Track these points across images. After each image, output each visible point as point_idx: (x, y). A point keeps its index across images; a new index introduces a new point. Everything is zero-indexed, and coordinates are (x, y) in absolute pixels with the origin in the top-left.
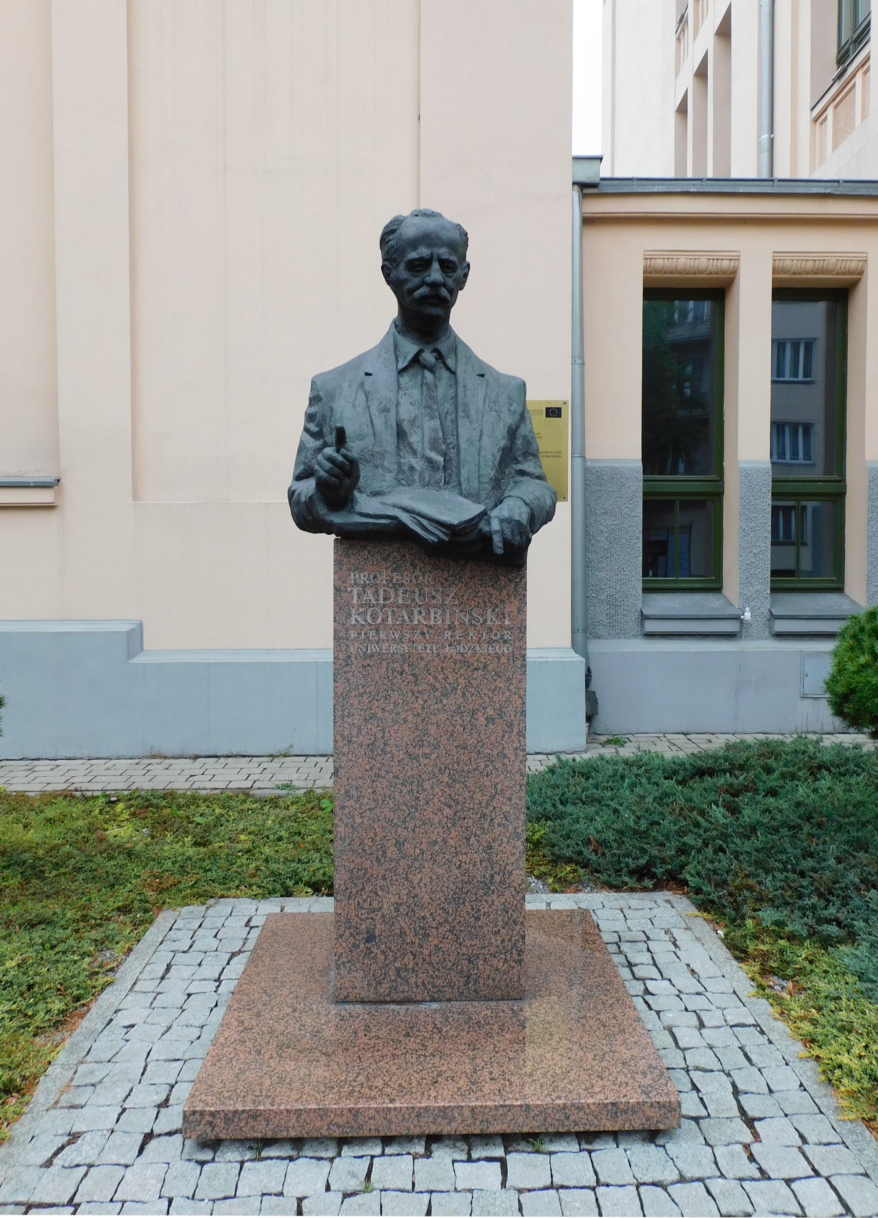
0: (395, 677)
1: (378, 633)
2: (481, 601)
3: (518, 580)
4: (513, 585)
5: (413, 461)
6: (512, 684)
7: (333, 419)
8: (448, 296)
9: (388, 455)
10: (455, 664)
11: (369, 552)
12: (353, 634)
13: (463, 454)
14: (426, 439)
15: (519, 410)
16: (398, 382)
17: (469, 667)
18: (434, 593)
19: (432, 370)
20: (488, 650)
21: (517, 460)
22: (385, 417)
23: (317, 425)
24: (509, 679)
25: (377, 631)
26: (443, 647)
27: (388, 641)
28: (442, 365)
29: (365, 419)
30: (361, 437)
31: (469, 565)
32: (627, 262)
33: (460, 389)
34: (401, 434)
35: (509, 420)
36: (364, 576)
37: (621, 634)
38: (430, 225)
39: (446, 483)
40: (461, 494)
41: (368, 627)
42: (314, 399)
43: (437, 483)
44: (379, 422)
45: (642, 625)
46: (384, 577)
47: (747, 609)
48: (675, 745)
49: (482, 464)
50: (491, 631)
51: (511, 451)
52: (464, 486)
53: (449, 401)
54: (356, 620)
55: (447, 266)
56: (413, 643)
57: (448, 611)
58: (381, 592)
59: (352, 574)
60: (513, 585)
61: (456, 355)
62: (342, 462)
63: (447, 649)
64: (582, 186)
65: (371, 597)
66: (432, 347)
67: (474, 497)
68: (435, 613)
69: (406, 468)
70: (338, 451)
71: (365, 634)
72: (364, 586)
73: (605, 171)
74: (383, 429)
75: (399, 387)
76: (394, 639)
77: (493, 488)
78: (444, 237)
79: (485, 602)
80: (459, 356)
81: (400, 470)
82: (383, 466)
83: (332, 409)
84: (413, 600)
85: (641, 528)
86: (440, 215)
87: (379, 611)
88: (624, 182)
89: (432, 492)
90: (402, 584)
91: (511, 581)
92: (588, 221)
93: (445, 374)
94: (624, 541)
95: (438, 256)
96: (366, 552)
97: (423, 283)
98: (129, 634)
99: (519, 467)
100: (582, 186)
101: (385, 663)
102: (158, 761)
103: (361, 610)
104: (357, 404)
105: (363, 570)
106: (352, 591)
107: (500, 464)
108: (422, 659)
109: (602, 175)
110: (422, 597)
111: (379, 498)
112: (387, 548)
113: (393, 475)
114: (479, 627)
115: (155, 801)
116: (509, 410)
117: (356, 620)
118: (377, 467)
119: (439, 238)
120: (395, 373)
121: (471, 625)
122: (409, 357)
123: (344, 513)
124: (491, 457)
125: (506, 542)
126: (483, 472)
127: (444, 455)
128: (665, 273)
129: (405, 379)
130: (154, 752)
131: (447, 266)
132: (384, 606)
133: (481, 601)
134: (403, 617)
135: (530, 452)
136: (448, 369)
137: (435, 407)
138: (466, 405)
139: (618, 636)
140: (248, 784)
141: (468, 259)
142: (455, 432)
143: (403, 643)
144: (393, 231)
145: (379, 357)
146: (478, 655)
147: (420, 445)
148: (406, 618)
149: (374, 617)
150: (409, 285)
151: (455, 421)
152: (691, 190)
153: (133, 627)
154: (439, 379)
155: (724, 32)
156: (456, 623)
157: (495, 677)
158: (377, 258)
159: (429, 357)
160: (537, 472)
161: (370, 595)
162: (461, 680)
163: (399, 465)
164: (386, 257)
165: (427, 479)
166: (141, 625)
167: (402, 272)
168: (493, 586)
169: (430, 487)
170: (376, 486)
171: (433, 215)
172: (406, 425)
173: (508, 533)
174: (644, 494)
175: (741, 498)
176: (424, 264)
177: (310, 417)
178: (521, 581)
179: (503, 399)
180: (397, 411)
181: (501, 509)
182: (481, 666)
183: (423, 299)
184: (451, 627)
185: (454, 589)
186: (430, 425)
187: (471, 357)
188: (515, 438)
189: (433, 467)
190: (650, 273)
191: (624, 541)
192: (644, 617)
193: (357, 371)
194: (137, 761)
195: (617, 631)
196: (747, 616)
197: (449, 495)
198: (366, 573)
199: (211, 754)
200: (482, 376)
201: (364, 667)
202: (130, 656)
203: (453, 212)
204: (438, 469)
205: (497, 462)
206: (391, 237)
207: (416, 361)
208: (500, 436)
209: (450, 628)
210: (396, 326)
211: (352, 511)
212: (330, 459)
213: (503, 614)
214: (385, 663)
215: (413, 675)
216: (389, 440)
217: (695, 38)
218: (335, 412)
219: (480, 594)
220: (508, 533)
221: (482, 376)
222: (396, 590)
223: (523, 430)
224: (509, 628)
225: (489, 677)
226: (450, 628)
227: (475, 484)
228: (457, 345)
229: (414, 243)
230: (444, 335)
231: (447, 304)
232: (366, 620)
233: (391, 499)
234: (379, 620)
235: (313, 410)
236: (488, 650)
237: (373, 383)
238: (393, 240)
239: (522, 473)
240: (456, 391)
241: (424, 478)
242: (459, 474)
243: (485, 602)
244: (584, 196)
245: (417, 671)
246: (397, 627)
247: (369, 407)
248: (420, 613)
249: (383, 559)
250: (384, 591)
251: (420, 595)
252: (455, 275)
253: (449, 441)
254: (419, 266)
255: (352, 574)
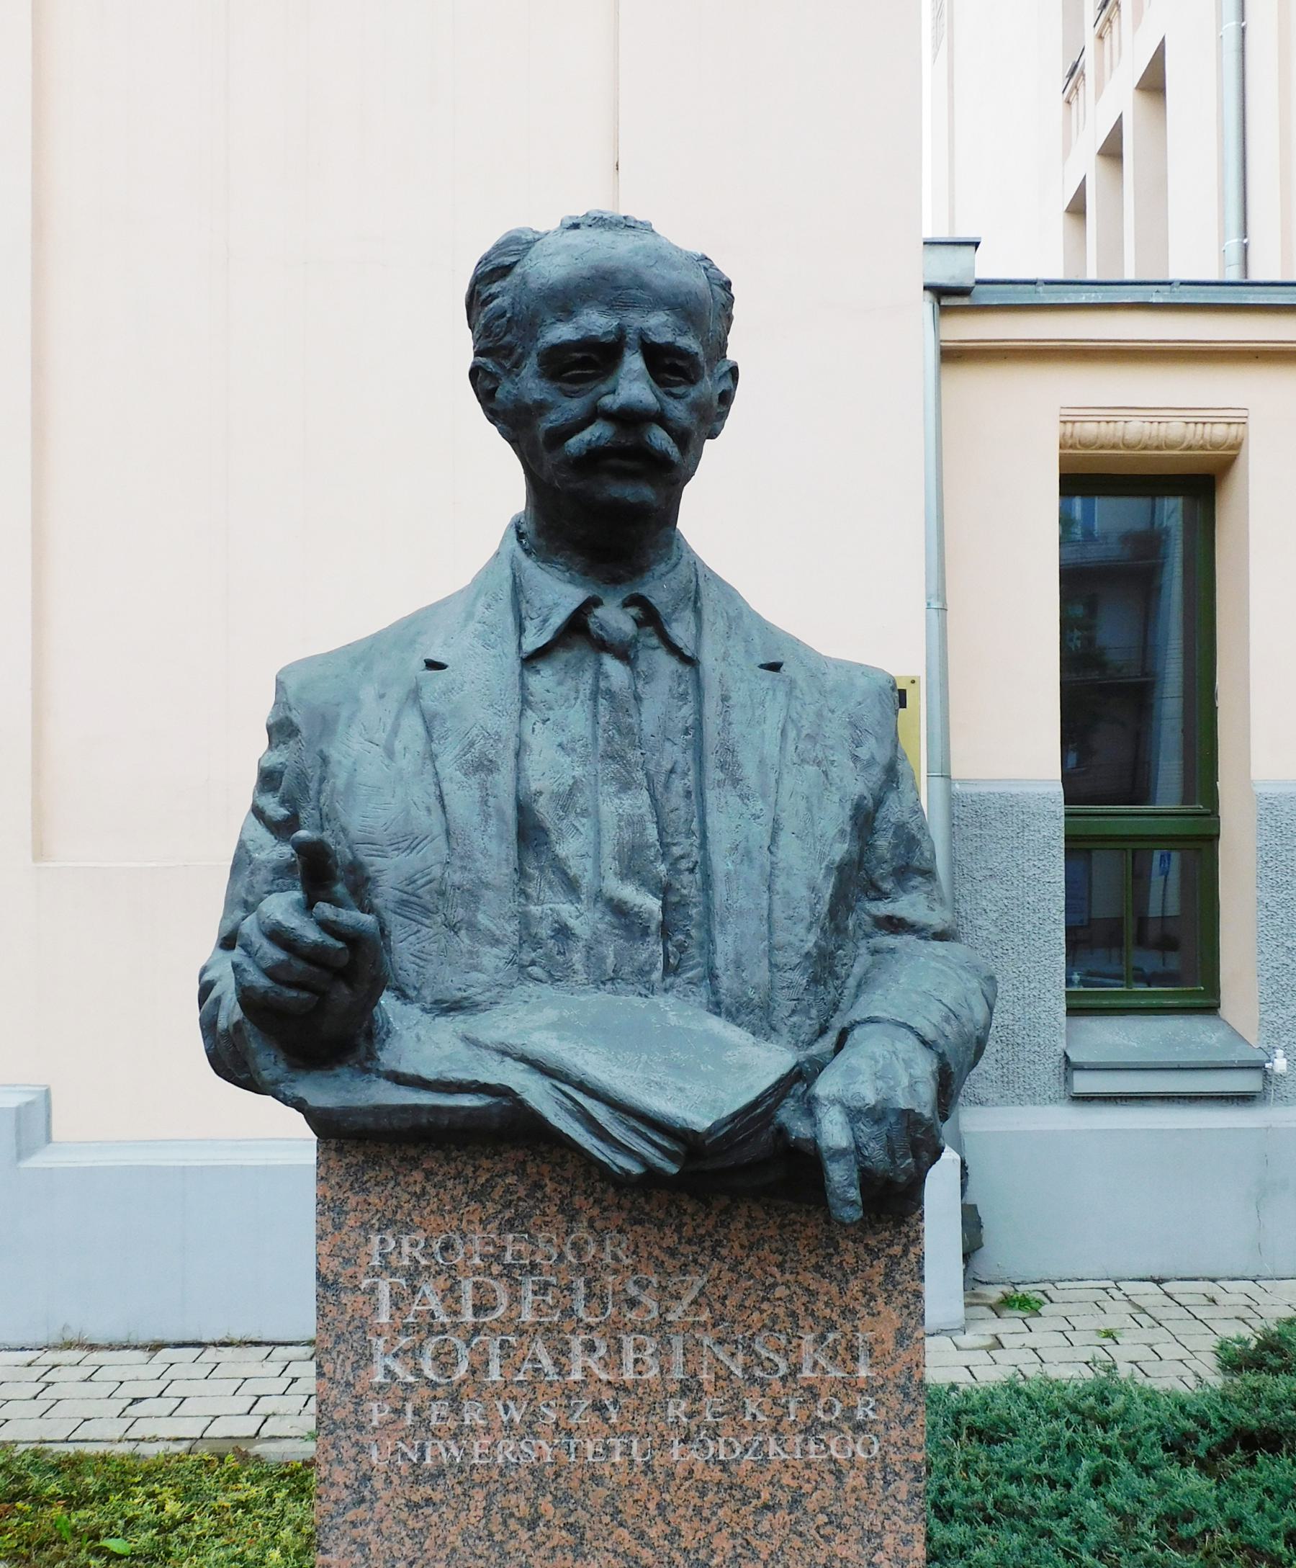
0: (513, 1535)
1: (457, 1411)
2: (781, 1311)
3: (897, 1250)
4: (880, 1264)
5: (566, 910)
6: (880, 1547)
7: (327, 788)
8: (674, 452)
9: (489, 895)
10: (703, 1495)
11: (429, 1174)
12: (377, 1413)
13: (720, 891)
14: (608, 848)
15: (883, 757)
16: (523, 686)
17: (745, 1502)
18: (633, 1291)
19: (625, 653)
20: (804, 1452)
21: (878, 889)
22: (483, 787)
23: (283, 803)
24: (870, 1534)
25: (455, 1401)
26: (665, 1444)
27: (488, 1430)
28: (654, 641)
29: (421, 793)
30: (410, 841)
31: (744, 1210)
32: (1027, 427)
33: (712, 707)
34: (530, 833)
35: (857, 786)
36: (414, 1244)
37: (1030, 1096)
38: (616, 249)
39: (669, 970)
40: (716, 1007)
41: (426, 1392)
42: (281, 730)
43: (642, 973)
44: (463, 799)
45: (1067, 1080)
46: (477, 1246)
47: (1280, 1052)
48: (1143, 1311)
49: (778, 914)
50: (816, 1397)
51: (861, 862)
52: (725, 982)
53: (680, 739)
54: (389, 1372)
55: (667, 365)
56: (569, 1434)
57: (677, 1342)
58: (467, 1287)
59: (375, 1239)
60: (880, 1264)
61: (698, 612)
62: (316, 945)
63: (676, 1450)
64: (939, 292)
65: (434, 1303)
66: (625, 592)
67: (755, 1015)
68: (638, 1348)
69: (544, 931)
70: (308, 906)
71: (417, 1412)
72: (413, 1274)
73: (986, 265)
74: (476, 819)
75: (525, 702)
76: (510, 1425)
77: (815, 980)
78: (657, 282)
79: (793, 1314)
80: (707, 614)
81: (527, 937)
82: (472, 926)
83: (325, 760)
84: (568, 1312)
85: (1063, 903)
86: (647, 228)
87: (460, 1344)
88: (1020, 287)
89: (630, 1002)
90: (533, 1265)
91: (874, 1254)
92: (951, 355)
93: (665, 664)
94: (1028, 927)
95: (642, 334)
96: (418, 1176)
97: (595, 414)
98: (21, 1113)
99: (883, 909)
100: (939, 292)
101: (479, 1495)
102: (75, 1355)
103: (403, 1342)
104: (398, 746)
105: (408, 1228)
106: (373, 1290)
107: (832, 913)
108: (597, 1479)
109: (980, 275)
110: (595, 1303)
111: (458, 1023)
112: (486, 1163)
113: (504, 951)
114: (777, 1386)
115: (35, 1481)
116: (855, 758)
117: (389, 1372)
118: (453, 928)
119: (643, 286)
120: (512, 662)
121: (752, 1380)
122: (557, 620)
123: (344, 1072)
124: (804, 892)
125: (867, 1179)
126: (780, 937)
127: (664, 890)
128: (1102, 447)
129: (543, 681)
130: (71, 1336)
131: (667, 365)
132: (477, 1330)
133: (781, 1311)
134: (535, 1360)
135: (911, 867)
136: (674, 650)
137: (634, 756)
138: (730, 751)
139: (1019, 1100)
140: (247, 1427)
141: (731, 355)
142: (695, 826)
143: (536, 1435)
144: (504, 271)
145: (470, 616)
146: (777, 1466)
147: (589, 863)
148: (546, 1363)
149: (445, 1362)
150: (553, 419)
151: (697, 795)
152: (1154, 300)
153: (29, 1098)
154: (648, 679)
155: (1153, 84)
156: (704, 1376)
157: (828, 1530)
158: (461, 348)
159: (615, 618)
160: (937, 918)
161: (431, 1295)
162: (722, 1542)
163: (525, 921)
164: (485, 343)
165: (611, 961)
166: (47, 1093)
167: (530, 384)
168: (818, 1268)
169: (620, 985)
170: (451, 983)
171: (626, 224)
172: (545, 810)
173: (875, 1151)
174: (1068, 839)
175: (1260, 849)
176: (598, 358)
177: (269, 779)
178: (905, 1252)
179: (836, 730)
180: (519, 769)
181: (851, 1073)
182: (784, 1497)
183: (593, 459)
184: (690, 1389)
185: (697, 1281)
186: (619, 808)
187: (739, 615)
188: (873, 831)
189: (627, 928)
190: (1071, 447)
191: (1028, 927)
192: (1070, 1066)
193: (408, 660)
194: (28, 1356)
195: (1016, 1090)
196: (1280, 1064)
197: (678, 1012)
198: (420, 1236)
199: (188, 1339)
200: (775, 667)
201: (413, 1506)
202: (19, 1156)
203: (686, 221)
204: (645, 932)
205: (823, 908)
206: (495, 288)
207: (577, 629)
208: (832, 832)
209: (685, 1390)
210: (520, 536)
211: (368, 1067)
212: (277, 935)
213: (850, 1347)
214: (479, 1495)
215: (570, 1528)
216: (493, 852)
217: (1098, 94)
218: (333, 768)
219: (781, 1292)
220: (875, 1151)
221: (775, 667)
222: (515, 1284)
223: (894, 810)
224: (870, 1389)
225: (807, 1528)
226: (685, 1390)
227: (760, 974)
228: (698, 589)
229: (565, 299)
230: (661, 559)
231: (670, 475)
232: (418, 1372)
233: (500, 1025)
234: (461, 1371)
235: (277, 758)
236: (804, 1452)
237: (448, 691)
238: (503, 295)
239: (895, 925)
240: (699, 712)
241: (602, 959)
242: (708, 944)
243: (793, 1314)
244: (944, 311)
245: (581, 1516)
246: (516, 1391)
247: (433, 757)
248: (590, 1348)
249: (473, 1196)
250: (477, 1286)
251: (589, 1297)
252: (694, 393)
253: (677, 851)
254: (583, 363)
255: (375, 1239)
